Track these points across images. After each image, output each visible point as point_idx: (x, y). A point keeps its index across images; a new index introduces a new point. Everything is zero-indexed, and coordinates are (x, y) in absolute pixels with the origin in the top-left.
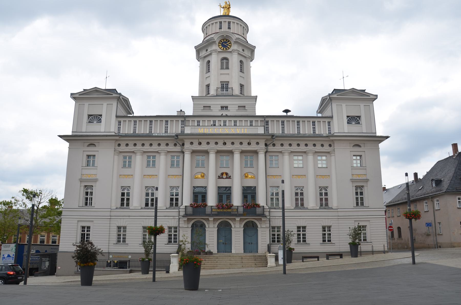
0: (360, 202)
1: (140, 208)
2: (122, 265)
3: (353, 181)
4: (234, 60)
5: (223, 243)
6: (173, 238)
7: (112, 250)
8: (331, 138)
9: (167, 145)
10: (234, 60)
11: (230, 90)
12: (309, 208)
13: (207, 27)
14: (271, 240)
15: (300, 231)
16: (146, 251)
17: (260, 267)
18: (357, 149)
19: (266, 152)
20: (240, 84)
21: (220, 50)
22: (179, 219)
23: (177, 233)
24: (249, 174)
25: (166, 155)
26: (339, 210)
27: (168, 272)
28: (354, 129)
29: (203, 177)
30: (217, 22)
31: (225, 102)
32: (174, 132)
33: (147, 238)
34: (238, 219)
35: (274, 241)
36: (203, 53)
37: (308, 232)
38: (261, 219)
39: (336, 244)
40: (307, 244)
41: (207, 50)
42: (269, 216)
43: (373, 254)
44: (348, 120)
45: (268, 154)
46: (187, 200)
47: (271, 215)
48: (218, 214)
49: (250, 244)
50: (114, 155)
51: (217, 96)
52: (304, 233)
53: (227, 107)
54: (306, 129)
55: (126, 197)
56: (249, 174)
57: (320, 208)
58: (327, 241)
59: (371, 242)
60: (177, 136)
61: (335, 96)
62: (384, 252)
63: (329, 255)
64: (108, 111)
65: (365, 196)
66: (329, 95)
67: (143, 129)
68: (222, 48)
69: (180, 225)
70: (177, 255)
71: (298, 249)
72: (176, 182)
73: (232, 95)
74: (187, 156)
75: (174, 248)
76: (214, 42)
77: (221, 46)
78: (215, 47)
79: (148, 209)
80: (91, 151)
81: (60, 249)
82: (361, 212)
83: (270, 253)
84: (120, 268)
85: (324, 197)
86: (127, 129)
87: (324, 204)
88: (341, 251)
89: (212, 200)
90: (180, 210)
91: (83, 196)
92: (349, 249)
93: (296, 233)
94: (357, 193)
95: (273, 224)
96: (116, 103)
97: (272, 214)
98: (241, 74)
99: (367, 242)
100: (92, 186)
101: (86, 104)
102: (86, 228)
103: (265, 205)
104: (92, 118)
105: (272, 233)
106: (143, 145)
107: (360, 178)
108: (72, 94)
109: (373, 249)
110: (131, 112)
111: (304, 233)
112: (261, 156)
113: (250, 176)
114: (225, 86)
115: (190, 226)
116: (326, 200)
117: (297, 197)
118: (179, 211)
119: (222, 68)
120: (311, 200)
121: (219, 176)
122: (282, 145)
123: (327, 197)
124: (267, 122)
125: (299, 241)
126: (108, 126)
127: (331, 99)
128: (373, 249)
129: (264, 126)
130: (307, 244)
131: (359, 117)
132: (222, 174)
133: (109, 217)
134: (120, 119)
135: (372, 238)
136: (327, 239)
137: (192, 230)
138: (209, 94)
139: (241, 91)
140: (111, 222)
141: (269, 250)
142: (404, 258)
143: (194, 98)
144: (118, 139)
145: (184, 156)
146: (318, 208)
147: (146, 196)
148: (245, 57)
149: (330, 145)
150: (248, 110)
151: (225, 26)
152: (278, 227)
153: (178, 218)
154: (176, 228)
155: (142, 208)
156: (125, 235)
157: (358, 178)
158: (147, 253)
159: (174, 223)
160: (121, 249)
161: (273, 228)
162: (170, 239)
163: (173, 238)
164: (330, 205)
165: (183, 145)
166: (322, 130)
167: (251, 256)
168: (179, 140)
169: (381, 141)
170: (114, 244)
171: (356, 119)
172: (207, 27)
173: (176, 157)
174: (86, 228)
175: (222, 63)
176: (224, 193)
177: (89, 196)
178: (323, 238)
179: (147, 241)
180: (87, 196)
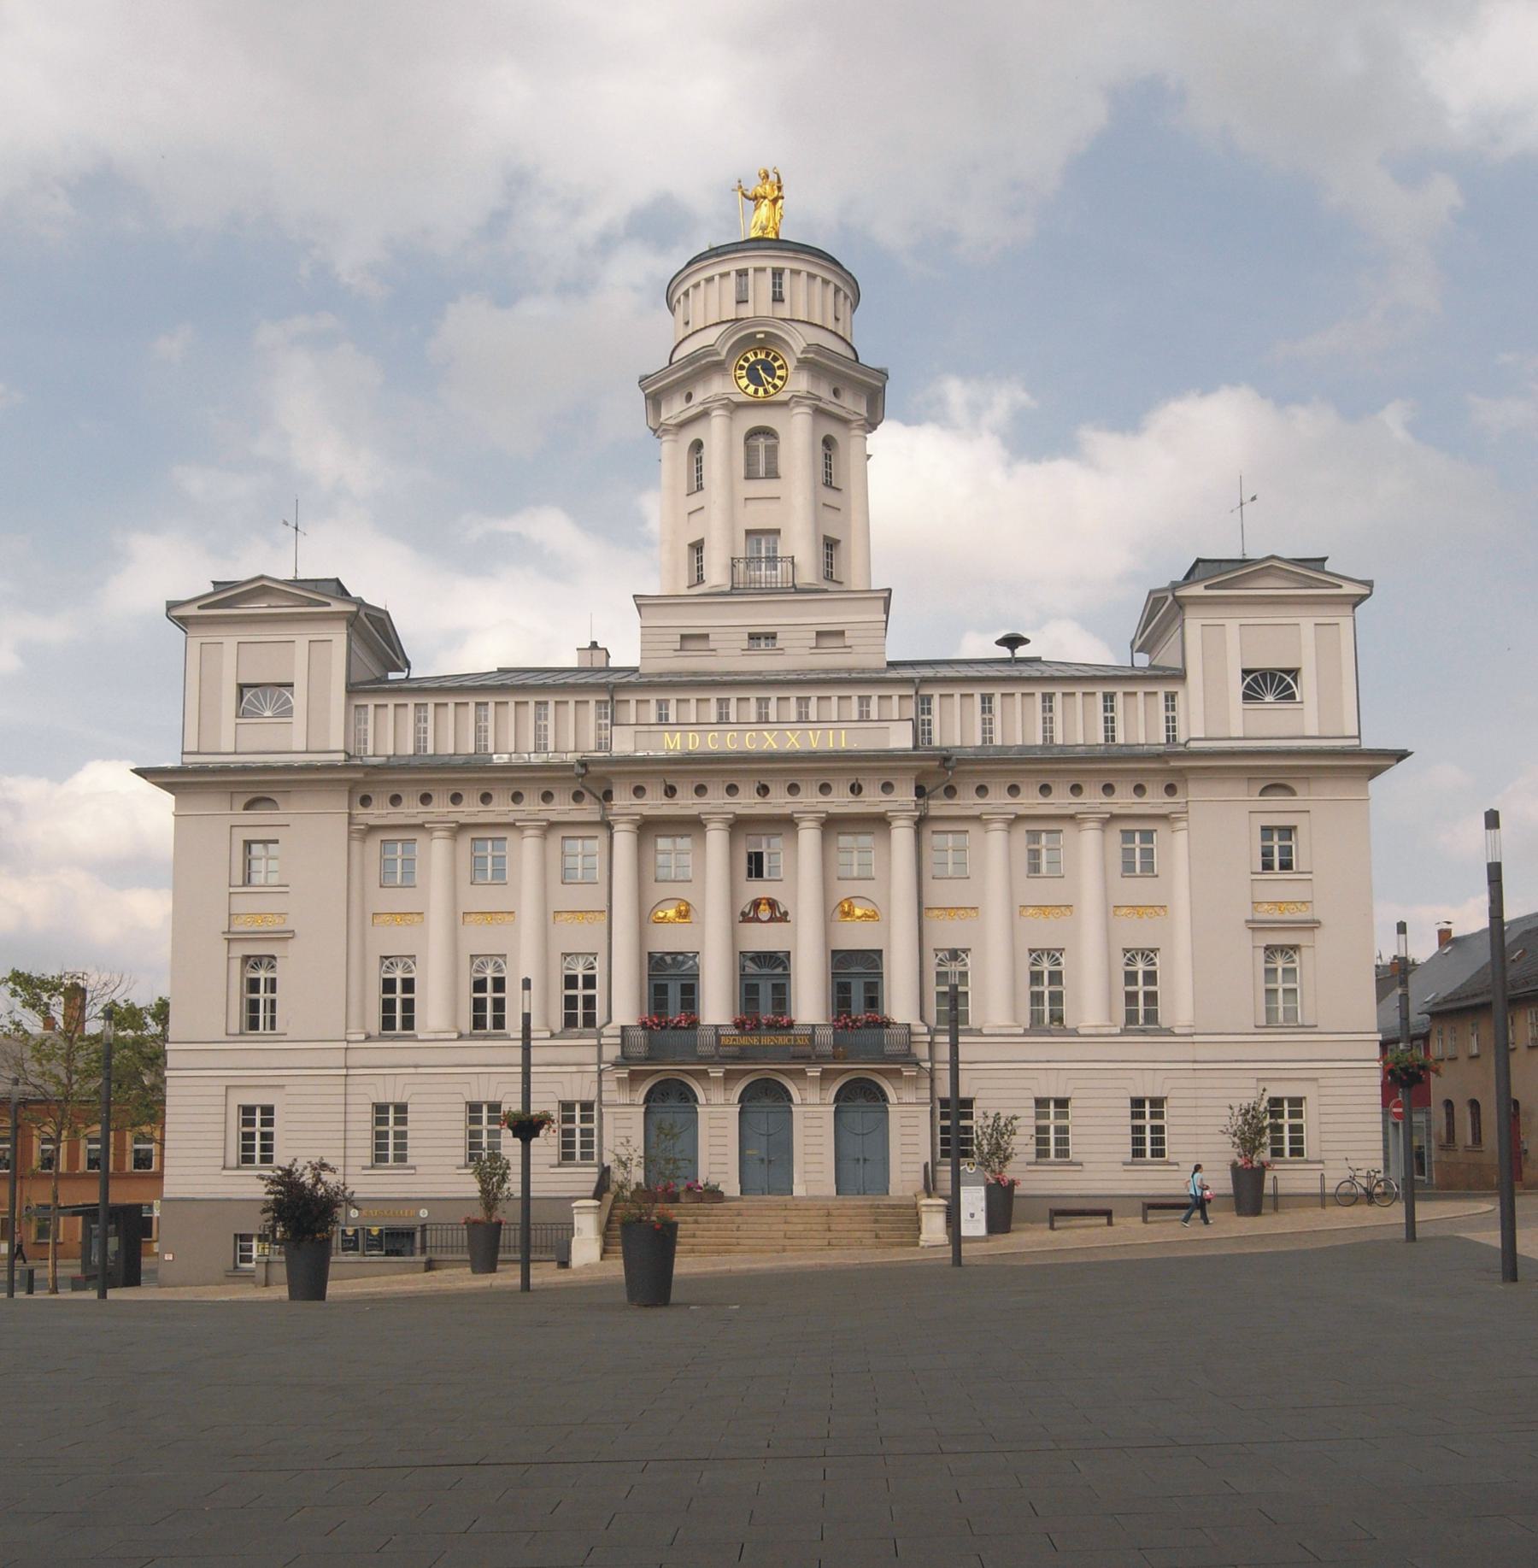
2: (397, 1241)
3: (1255, 926)
6: (578, 1145)
10: (797, 435)
12: (1081, 1031)
13: (686, 294)
14: (939, 1148)
16: (483, 1191)
17: (893, 1245)
18: (1277, 801)
20: (825, 537)
21: (742, 398)
22: (600, 1072)
23: (594, 1125)
27: (564, 1264)
28: (1271, 724)
29: (685, 917)
30: (728, 274)
31: (763, 618)
33: (485, 1145)
34: (814, 1072)
36: (675, 409)
37: (1309, 1121)
40: (1071, 1163)
41: (689, 397)
44: (1248, 687)
46: (623, 1004)
48: (742, 1055)
49: (859, 1161)
50: (350, 839)
54: (1078, 724)
55: (399, 996)
59: (1321, 1162)
61: (1198, 590)
63: (1154, 1206)
64: (318, 660)
66: (1175, 586)
67: (451, 733)
68: (751, 389)
69: (605, 1097)
70: (595, 1203)
71: (1034, 1180)
73: (797, 590)
75: (587, 1177)
77: (744, 382)
79: (486, 1037)
80: (1278, 809)
81: (165, 1189)
82: (1284, 1046)
83: (929, 1196)
84: (387, 1254)
85: (1141, 988)
86: (392, 733)
87: (1141, 1013)
90: (603, 1041)
92: (1230, 1184)
93: (1032, 1122)
94: (1270, 973)
98: (830, 497)
99: (1307, 1162)
100: (274, 957)
101: (229, 640)
103: (914, 1021)
104: (1255, 680)
107: (1287, 916)
108: (171, 606)
109: (1323, 1186)
113: (858, 912)
115: (640, 1096)
116: (1151, 998)
117: (1036, 989)
118: (600, 1046)
119: (750, 475)
120: (1091, 999)
121: (743, 914)
122: (982, 790)
123: (1152, 988)
124: (928, 699)
125: (1042, 1153)
127: (1180, 604)
131: (1294, 673)
132: (756, 904)
133: (344, 1072)
135: (1326, 1146)
137: (646, 1113)
138: (701, 580)
141: (930, 1188)
142: (1469, 1219)
144: (360, 781)
149: (1171, 789)
153: (595, 1068)
154: (587, 1106)
156: (401, 1135)
157: (1277, 916)
158: (490, 1198)
159: (580, 1088)
162: (567, 1145)
163: (578, 1145)
164: (1164, 1020)
165: (608, 796)
166: (1140, 723)
167: (859, 1207)
168: (593, 780)
169: (1374, 772)
170: (364, 1168)
171: (1282, 680)
172: (686, 294)
173: (1137, 836)
174: (258, 1111)
175: (750, 452)
176: (763, 976)
177: (262, 996)
178: (1161, 1141)
179: (485, 1155)
180: (254, 996)
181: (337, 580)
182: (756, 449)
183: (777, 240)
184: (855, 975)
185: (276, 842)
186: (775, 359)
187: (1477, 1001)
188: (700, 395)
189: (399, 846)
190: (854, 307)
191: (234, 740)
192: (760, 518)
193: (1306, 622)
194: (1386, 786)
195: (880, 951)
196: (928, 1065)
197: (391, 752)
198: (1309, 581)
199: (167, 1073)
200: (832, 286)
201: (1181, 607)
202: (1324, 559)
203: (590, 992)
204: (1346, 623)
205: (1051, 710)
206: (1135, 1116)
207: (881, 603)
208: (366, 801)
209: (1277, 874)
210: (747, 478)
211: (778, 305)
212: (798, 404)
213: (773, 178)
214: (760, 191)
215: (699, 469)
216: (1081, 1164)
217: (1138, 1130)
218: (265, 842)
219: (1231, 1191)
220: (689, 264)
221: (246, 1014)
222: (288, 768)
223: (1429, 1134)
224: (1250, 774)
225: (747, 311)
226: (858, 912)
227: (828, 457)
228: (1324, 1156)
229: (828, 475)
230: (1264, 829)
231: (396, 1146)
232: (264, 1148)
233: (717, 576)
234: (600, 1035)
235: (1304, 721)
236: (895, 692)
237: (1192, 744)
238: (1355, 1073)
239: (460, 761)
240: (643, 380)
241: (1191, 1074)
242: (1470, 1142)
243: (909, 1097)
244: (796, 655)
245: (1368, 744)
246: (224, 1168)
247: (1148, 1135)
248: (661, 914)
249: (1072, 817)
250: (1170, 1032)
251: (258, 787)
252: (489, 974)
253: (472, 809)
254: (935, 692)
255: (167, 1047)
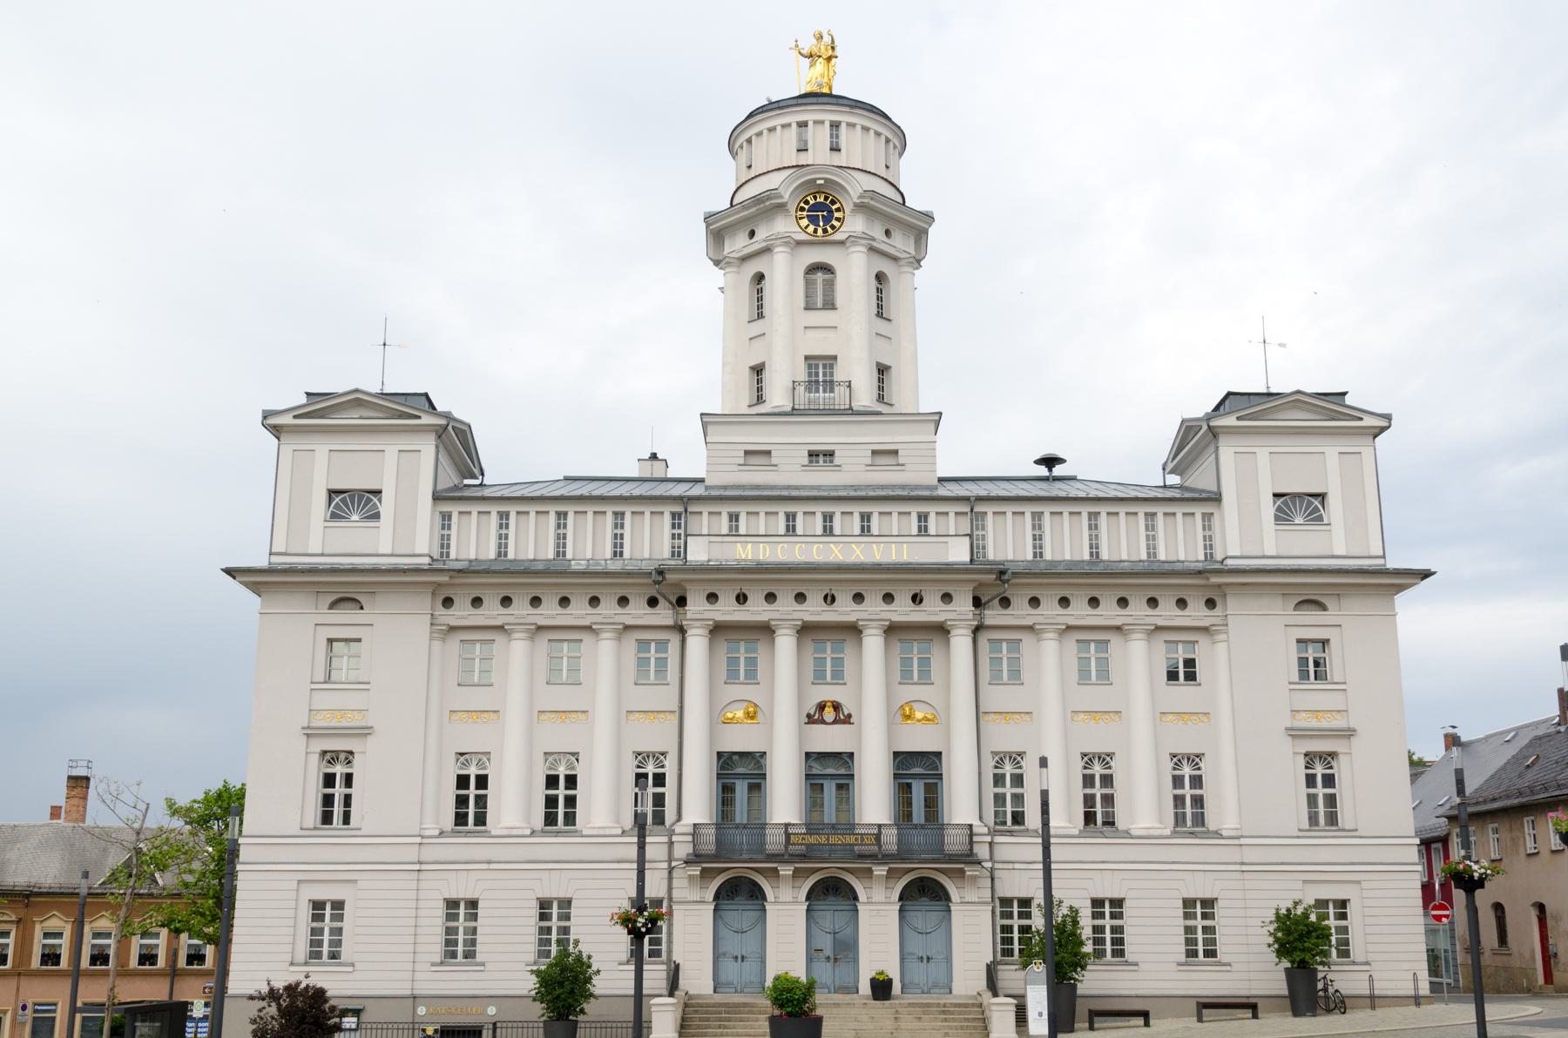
0: (1324, 808)
1: (528, 832)
3: (1295, 734)
4: (853, 271)
5: (828, 958)
7: (423, 988)
8: (1215, 580)
9: (623, 601)
10: (853, 271)
11: (840, 391)
12: (1134, 833)
13: (749, 141)
14: (999, 947)
15: (1102, 915)
18: (1312, 616)
19: (977, 630)
21: (803, 237)
22: (671, 870)
24: (915, 705)
25: (619, 639)
26: (1243, 841)
30: (789, 125)
32: (646, 555)
35: (1008, 953)
36: (738, 244)
37: (1130, 922)
38: (962, 871)
39: (1235, 967)
40: (1127, 963)
41: (752, 234)
42: (991, 859)
43: (1373, 1007)
44: (1279, 509)
45: (983, 638)
46: (696, 803)
47: (997, 857)
51: (794, 412)
52: (1117, 922)
53: (830, 454)
54: (1123, 542)
56: (915, 705)
57: (1175, 834)
58: (1201, 953)
59: (1367, 963)
60: (661, 572)
61: (1230, 421)
62: (1417, 1000)
63: (1207, 1006)
64: (405, 470)
65: (1342, 790)
66: (1208, 418)
67: (532, 541)
68: (811, 228)
69: (676, 894)
72: (657, 737)
73: (851, 411)
74: (697, 643)
76: (781, 207)
77: (805, 222)
78: (786, 226)
80: (1312, 624)
82: (1326, 849)
83: (995, 995)
85: (1187, 791)
86: (474, 540)
88: (1254, 992)
89: (784, 802)
91: (315, 790)
92: (1284, 985)
94: (1310, 781)
95: (1005, 890)
96: (432, 449)
97: (1002, 853)
98: (881, 326)
99: (1354, 963)
100: (351, 753)
102: (328, 907)
105: (1000, 922)
106: (536, 601)
107: (1324, 724)
108: (267, 415)
110: (476, 471)
111: (1117, 922)
112: (961, 643)
113: (919, 715)
114: (820, 369)
115: (710, 895)
116: (1198, 801)
117: (1089, 791)
118: (671, 843)
119: (809, 307)
120: (1143, 802)
121: (809, 716)
122: (1034, 602)
126: (405, 531)
127: (1214, 433)
128: (1372, 988)
129: (971, 536)
130: (1127, 963)
131: (1321, 497)
132: (821, 707)
133: (417, 867)
134: (446, 507)
136: (1201, 946)
137: (808, 910)
138: (760, 399)
139: (881, 388)
140: (423, 885)
141: (993, 986)
143: (707, 420)
144: (445, 584)
145: (683, 641)
146: (1168, 832)
147: (548, 787)
148: (895, 259)
149: (1211, 603)
150: (908, 467)
151: (819, 138)
152: (1025, 903)
153: (665, 865)
155: (533, 833)
157: (1314, 724)
160: (459, 980)
161: (1006, 902)
164: (1212, 823)
165: (682, 601)
166: (1179, 542)
168: (667, 587)
170: (433, 964)
171: (1310, 504)
173: (653, 645)
174: (328, 907)
175: (809, 285)
176: (829, 773)
181: (426, 395)
182: (814, 282)
183: (830, 95)
184: (917, 772)
185: (359, 640)
186: (833, 202)
187: (1496, 805)
188: (762, 233)
189: (1004, 645)
190: (901, 155)
191: (326, 541)
192: (820, 345)
193: (1331, 451)
194: (1410, 607)
195: (939, 754)
196: (989, 865)
197: (473, 557)
198: (1330, 413)
199: (239, 867)
200: (883, 139)
201: (1215, 436)
202: (1344, 394)
203: (659, 790)
204: (1367, 452)
205: (507, 526)
206: (1187, 916)
207: (932, 426)
208: (448, 602)
209: (1313, 685)
210: (806, 309)
211: (835, 154)
212: (854, 244)
213: (827, 39)
214: (815, 50)
215: (760, 299)
216: (1229, 964)
217: (1189, 930)
218: (347, 640)
219: (1286, 992)
220: (751, 115)
221: (320, 809)
222: (375, 571)
223: (1453, 937)
224: (1284, 591)
225: (804, 159)
226: (919, 715)
227: (879, 291)
228: (1371, 957)
229: (880, 307)
230: (1299, 641)
231: (456, 943)
232: (1115, 942)
233: (777, 397)
234: (671, 833)
235: (1333, 542)
236: (952, 509)
237: (1229, 562)
238: (1068, 874)
239: (540, 567)
240: (709, 218)
241: (1238, 875)
242: (1496, 945)
243: (972, 895)
244: (853, 470)
245: (1392, 563)
246: (292, 964)
247: (1108, 936)
248: (730, 715)
249: (1118, 628)
250: (1217, 834)
251: (345, 588)
252: (562, 771)
253: (549, 612)
254: (989, 509)
255: (241, 841)
